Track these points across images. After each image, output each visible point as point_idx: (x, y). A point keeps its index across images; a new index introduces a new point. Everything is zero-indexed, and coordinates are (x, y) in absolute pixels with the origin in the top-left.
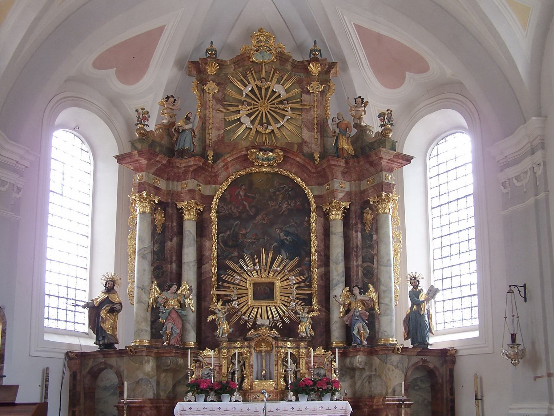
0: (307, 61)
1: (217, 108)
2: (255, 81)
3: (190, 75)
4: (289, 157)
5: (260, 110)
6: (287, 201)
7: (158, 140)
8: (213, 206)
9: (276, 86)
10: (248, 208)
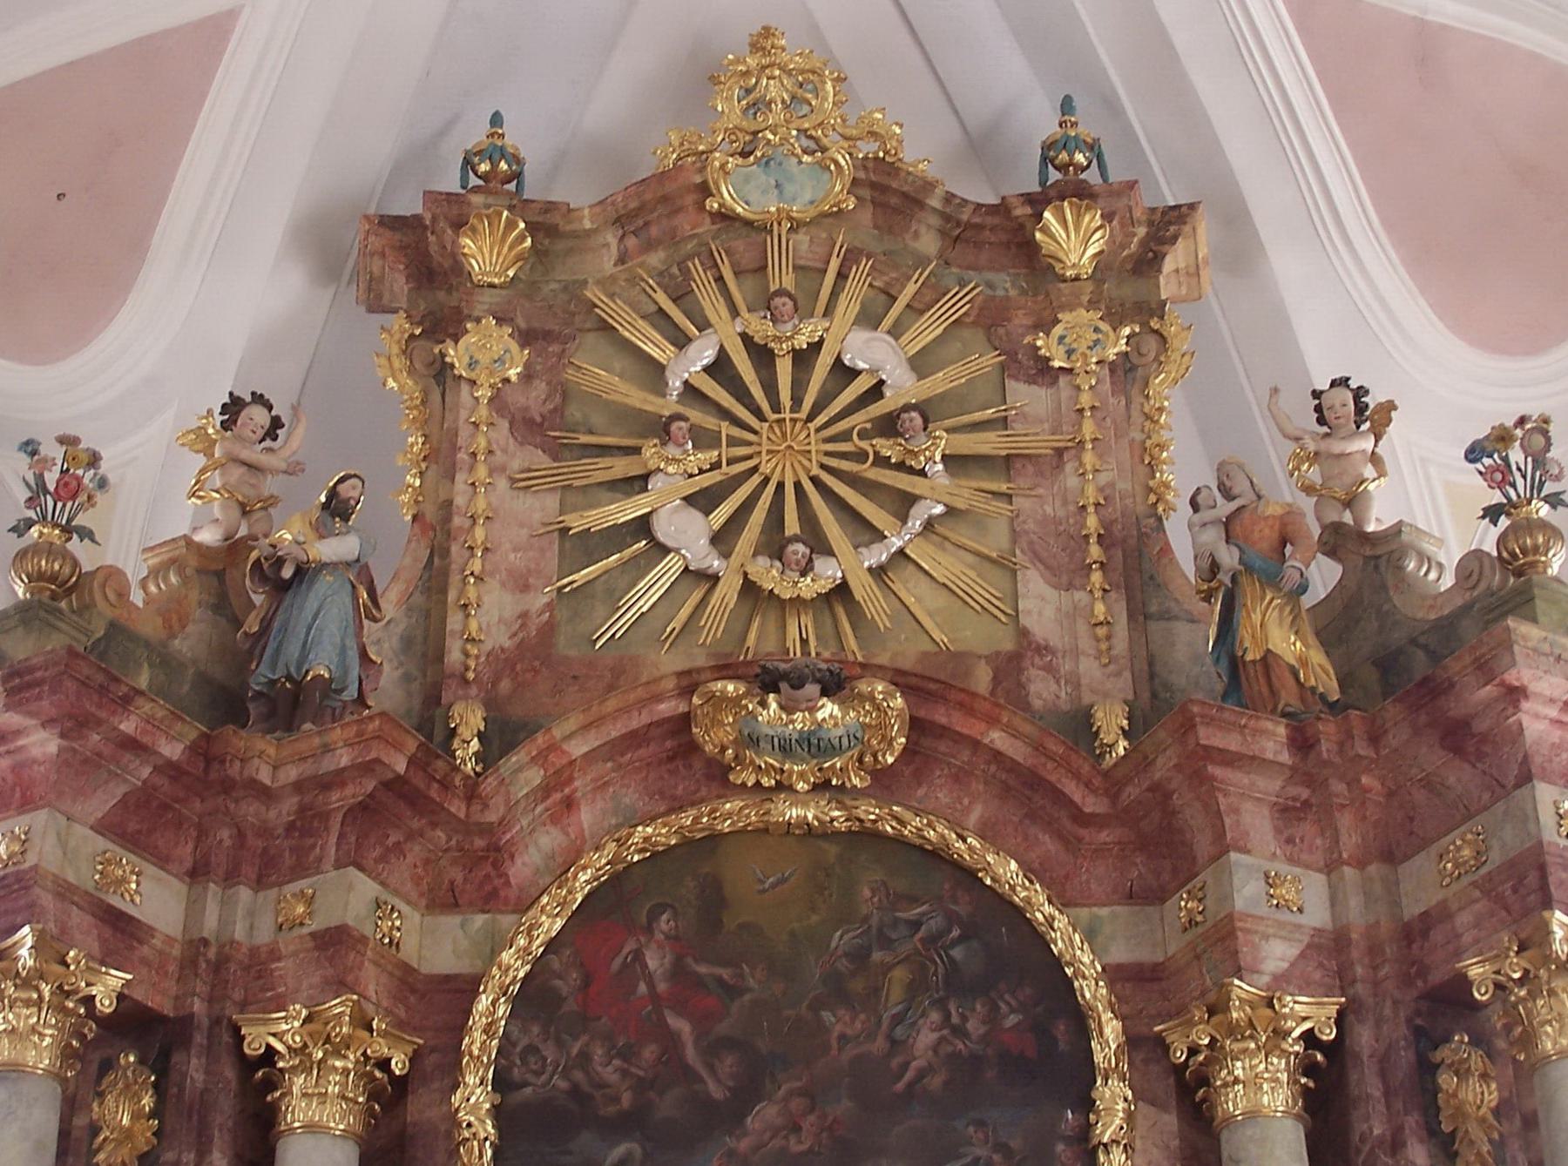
0: (1029, 199)
1: (516, 464)
2: (734, 312)
3: (376, 304)
4: (944, 732)
5: (766, 469)
6: (941, 1004)
7: (150, 628)
8: (474, 1041)
9: (859, 337)
10: (691, 1054)
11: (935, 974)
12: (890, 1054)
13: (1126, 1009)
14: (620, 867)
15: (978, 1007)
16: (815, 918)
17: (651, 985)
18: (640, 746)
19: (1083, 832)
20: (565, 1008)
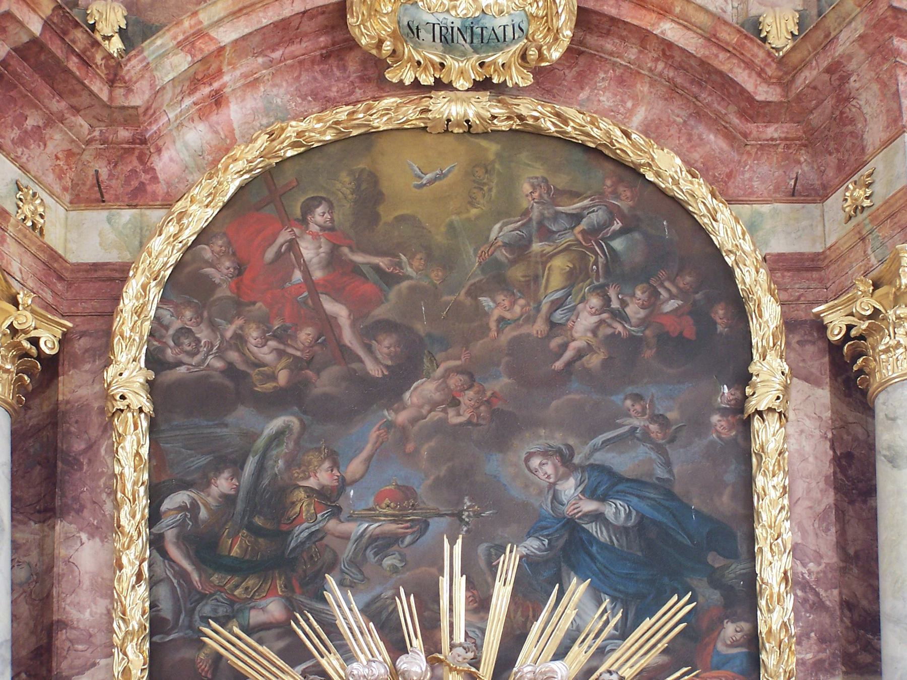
6: (601, 291)
10: (348, 337)
11: (596, 263)
12: (549, 337)
13: (784, 296)
14: (274, 161)
15: (638, 293)
16: (474, 211)
17: (307, 273)
18: (291, 42)
19: (751, 127)
20: (219, 294)
